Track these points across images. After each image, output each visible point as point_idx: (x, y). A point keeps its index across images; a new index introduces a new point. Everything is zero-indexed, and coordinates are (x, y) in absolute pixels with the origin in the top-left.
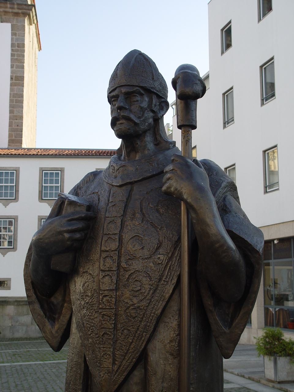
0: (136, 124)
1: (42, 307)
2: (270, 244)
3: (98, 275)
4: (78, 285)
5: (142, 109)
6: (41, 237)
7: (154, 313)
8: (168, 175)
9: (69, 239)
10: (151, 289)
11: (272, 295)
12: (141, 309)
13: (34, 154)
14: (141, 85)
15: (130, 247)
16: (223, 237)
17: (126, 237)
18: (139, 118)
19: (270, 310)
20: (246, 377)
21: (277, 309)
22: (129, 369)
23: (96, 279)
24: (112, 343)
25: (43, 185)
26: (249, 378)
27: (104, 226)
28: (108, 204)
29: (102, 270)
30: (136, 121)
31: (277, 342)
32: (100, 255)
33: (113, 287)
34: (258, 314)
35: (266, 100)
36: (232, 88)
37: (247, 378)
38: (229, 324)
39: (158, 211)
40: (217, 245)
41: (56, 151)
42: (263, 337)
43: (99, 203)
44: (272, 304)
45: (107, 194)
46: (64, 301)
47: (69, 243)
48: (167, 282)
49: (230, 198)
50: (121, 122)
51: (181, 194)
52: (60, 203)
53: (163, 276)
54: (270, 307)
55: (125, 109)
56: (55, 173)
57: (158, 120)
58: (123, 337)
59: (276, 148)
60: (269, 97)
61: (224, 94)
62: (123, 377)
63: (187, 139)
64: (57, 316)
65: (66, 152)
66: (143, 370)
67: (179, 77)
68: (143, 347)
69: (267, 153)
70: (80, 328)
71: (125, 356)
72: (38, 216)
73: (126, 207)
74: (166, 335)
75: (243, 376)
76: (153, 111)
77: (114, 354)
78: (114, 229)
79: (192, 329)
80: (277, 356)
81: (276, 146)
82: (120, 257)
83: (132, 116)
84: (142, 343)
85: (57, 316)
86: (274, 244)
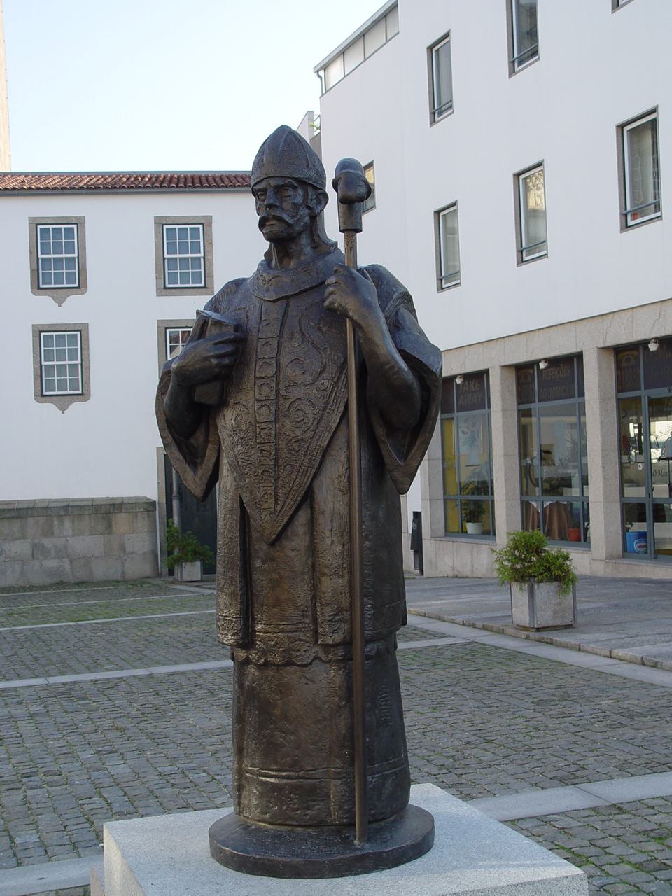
0: (289, 225)
1: (181, 451)
2: (531, 371)
3: (254, 406)
4: (228, 421)
5: (296, 206)
6: (184, 364)
7: (320, 446)
8: (331, 289)
9: (218, 365)
10: (315, 418)
11: (537, 480)
12: (304, 442)
13: (14, 189)
14: (294, 176)
15: (289, 372)
16: (393, 358)
17: (285, 360)
18: (293, 217)
19: (533, 505)
20: (479, 627)
21: (547, 504)
22: (294, 508)
23: (251, 411)
24: (273, 481)
25: (40, 256)
26: (484, 628)
27: (257, 349)
28: (260, 324)
29: (257, 400)
30: (290, 222)
31: (534, 556)
32: (255, 382)
33: (273, 418)
34: (508, 515)
35: (520, 63)
36: (447, 35)
37: (480, 629)
38: (405, 457)
39: (319, 329)
40: (387, 367)
41: (62, 180)
42: (508, 549)
43: (248, 321)
44: (537, 494)
45: (257, 311)
46: (207, 441)
47: (216, 370)
48: (334, 410)
49: (404, 312)
50: (271, 223)
51: (346, 310)
52: (202, 323)
53: (328, 404)
54: (532, 501)
55: (276, 206)
56: (53, 229)
57: (315, 219)
58: (286, 473)
59: (541, 168)
60: (525, 56)
61: (430, 48)
62: (288, 517)
63: (351, 246)
64: (199, 461)
65: (85, 181)
66: (309, 510)
67: (340, 178)
68: (308, 484)
69: (523, 179)
70: (235, 467)
71: (289, 494)
72: (33, 325)
73: (282, 325)
74: (334, 471)
75: (474, 626)
76: (309, 208)
77: (276, 493)
78: (270, 352)
79: (363, 461)
80: (534, 581)
81: (540, 164)
82: (279, 384)
83: (285, 217)
84: (307, 480)
85: (199, 461)
86: (540, 371)
